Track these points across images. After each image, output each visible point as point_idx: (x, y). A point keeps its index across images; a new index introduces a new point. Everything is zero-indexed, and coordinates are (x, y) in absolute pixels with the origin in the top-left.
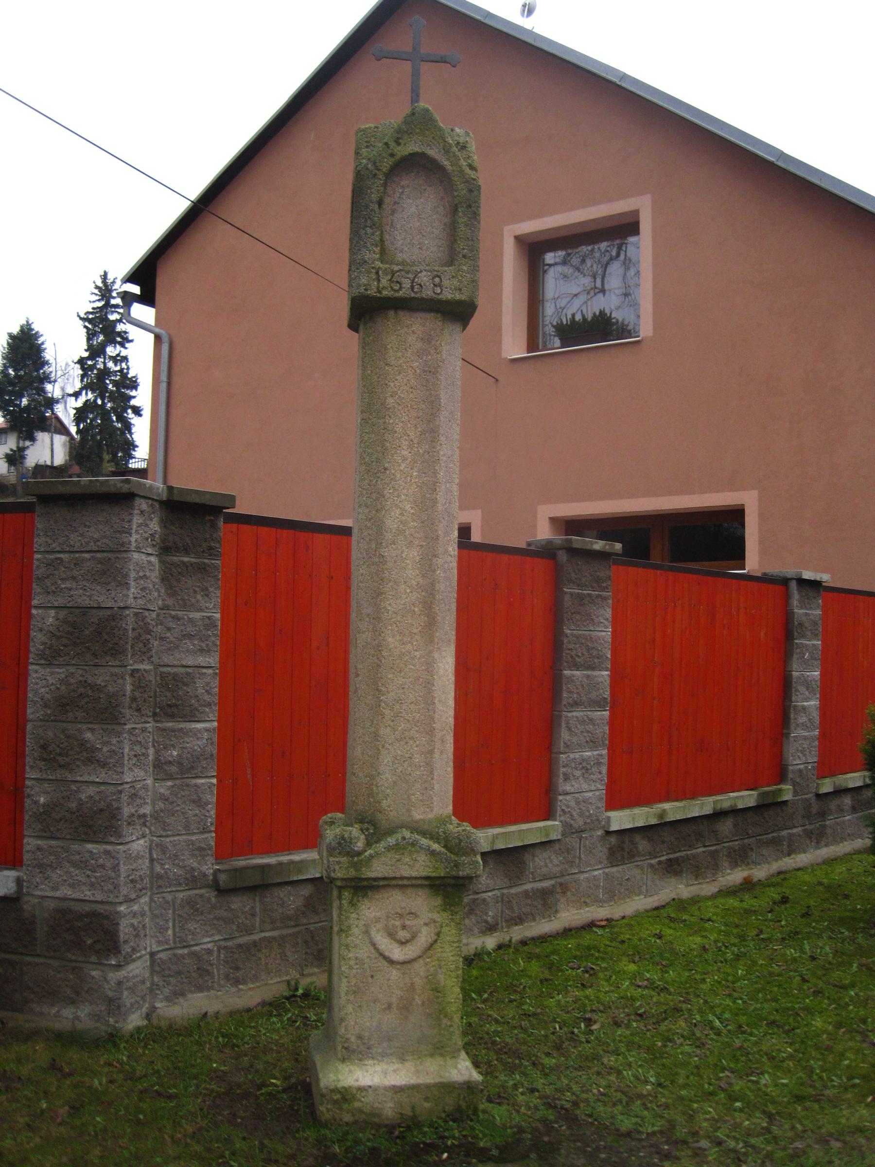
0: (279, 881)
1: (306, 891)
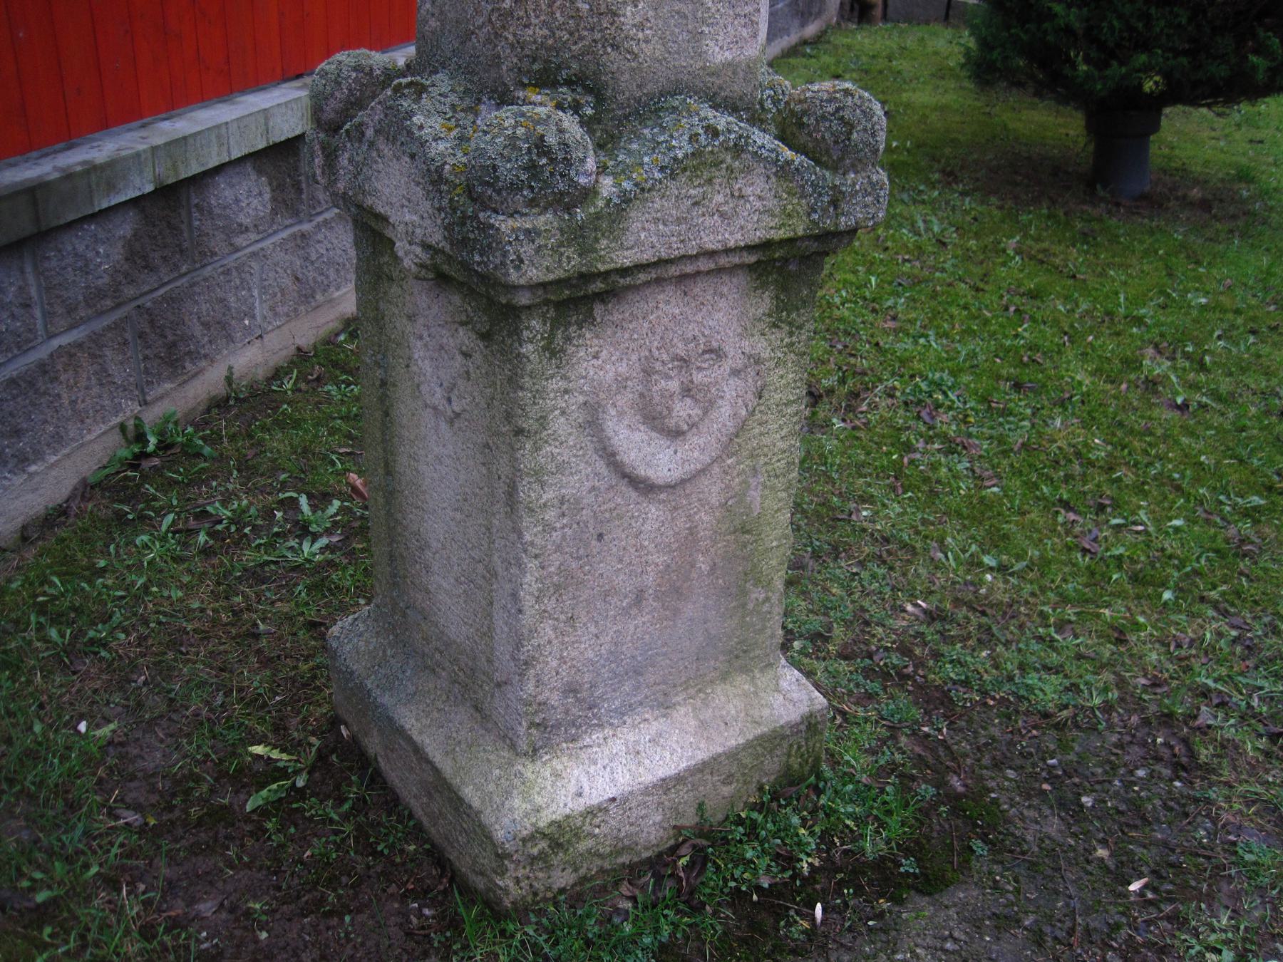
0: (71, 217)
1: (126, 227)
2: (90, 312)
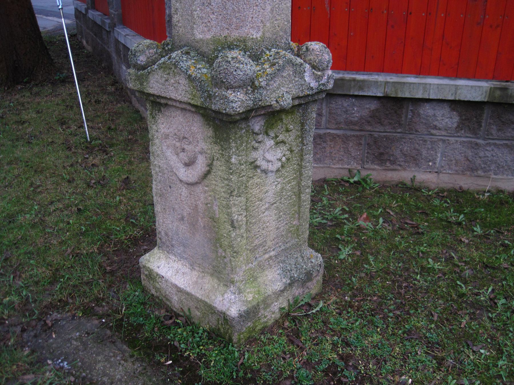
0: (339, 93)
2: (346, 127)
